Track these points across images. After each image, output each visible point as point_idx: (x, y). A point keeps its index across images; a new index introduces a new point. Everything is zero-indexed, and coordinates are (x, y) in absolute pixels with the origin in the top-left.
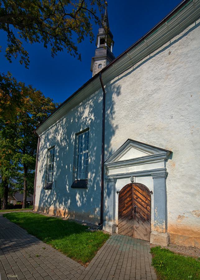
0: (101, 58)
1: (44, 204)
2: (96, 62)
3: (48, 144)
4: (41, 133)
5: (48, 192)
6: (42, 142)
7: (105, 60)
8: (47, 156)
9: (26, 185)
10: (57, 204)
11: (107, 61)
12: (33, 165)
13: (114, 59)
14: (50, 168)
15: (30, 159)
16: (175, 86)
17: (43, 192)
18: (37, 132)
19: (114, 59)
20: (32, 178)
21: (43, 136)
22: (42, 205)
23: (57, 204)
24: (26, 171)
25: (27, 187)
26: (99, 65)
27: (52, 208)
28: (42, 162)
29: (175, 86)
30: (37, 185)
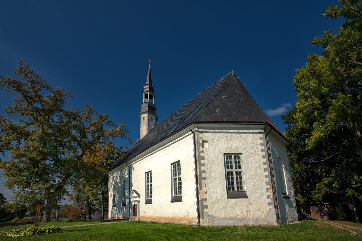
0: (145, 113)
1: (114, 215)
2: (142, 115)
3: (114, 183)
4: (110, 174)
5: (115, 208)
6: (111, 181)
7: (147, 114)
8: (113, 191)
9: (103, 205)
10: (119, 214)
11: (149, 114)
12: (107, 192)
13: (242, 190)
14: (114, 196)
15: (105, 190)
16: (260, 179)
17: (113, 209)
18: (108, 174)
19: (242, 190)
20: (107, 200)
21: (111, 177)
22: (112, 216)
23: (119, 214)
24: (103, 196)
25: (104, 206)
26: (144, 118)
27: (117, 216)
28: (111, 193)
29: (260, 179)
30: (109, 205)
